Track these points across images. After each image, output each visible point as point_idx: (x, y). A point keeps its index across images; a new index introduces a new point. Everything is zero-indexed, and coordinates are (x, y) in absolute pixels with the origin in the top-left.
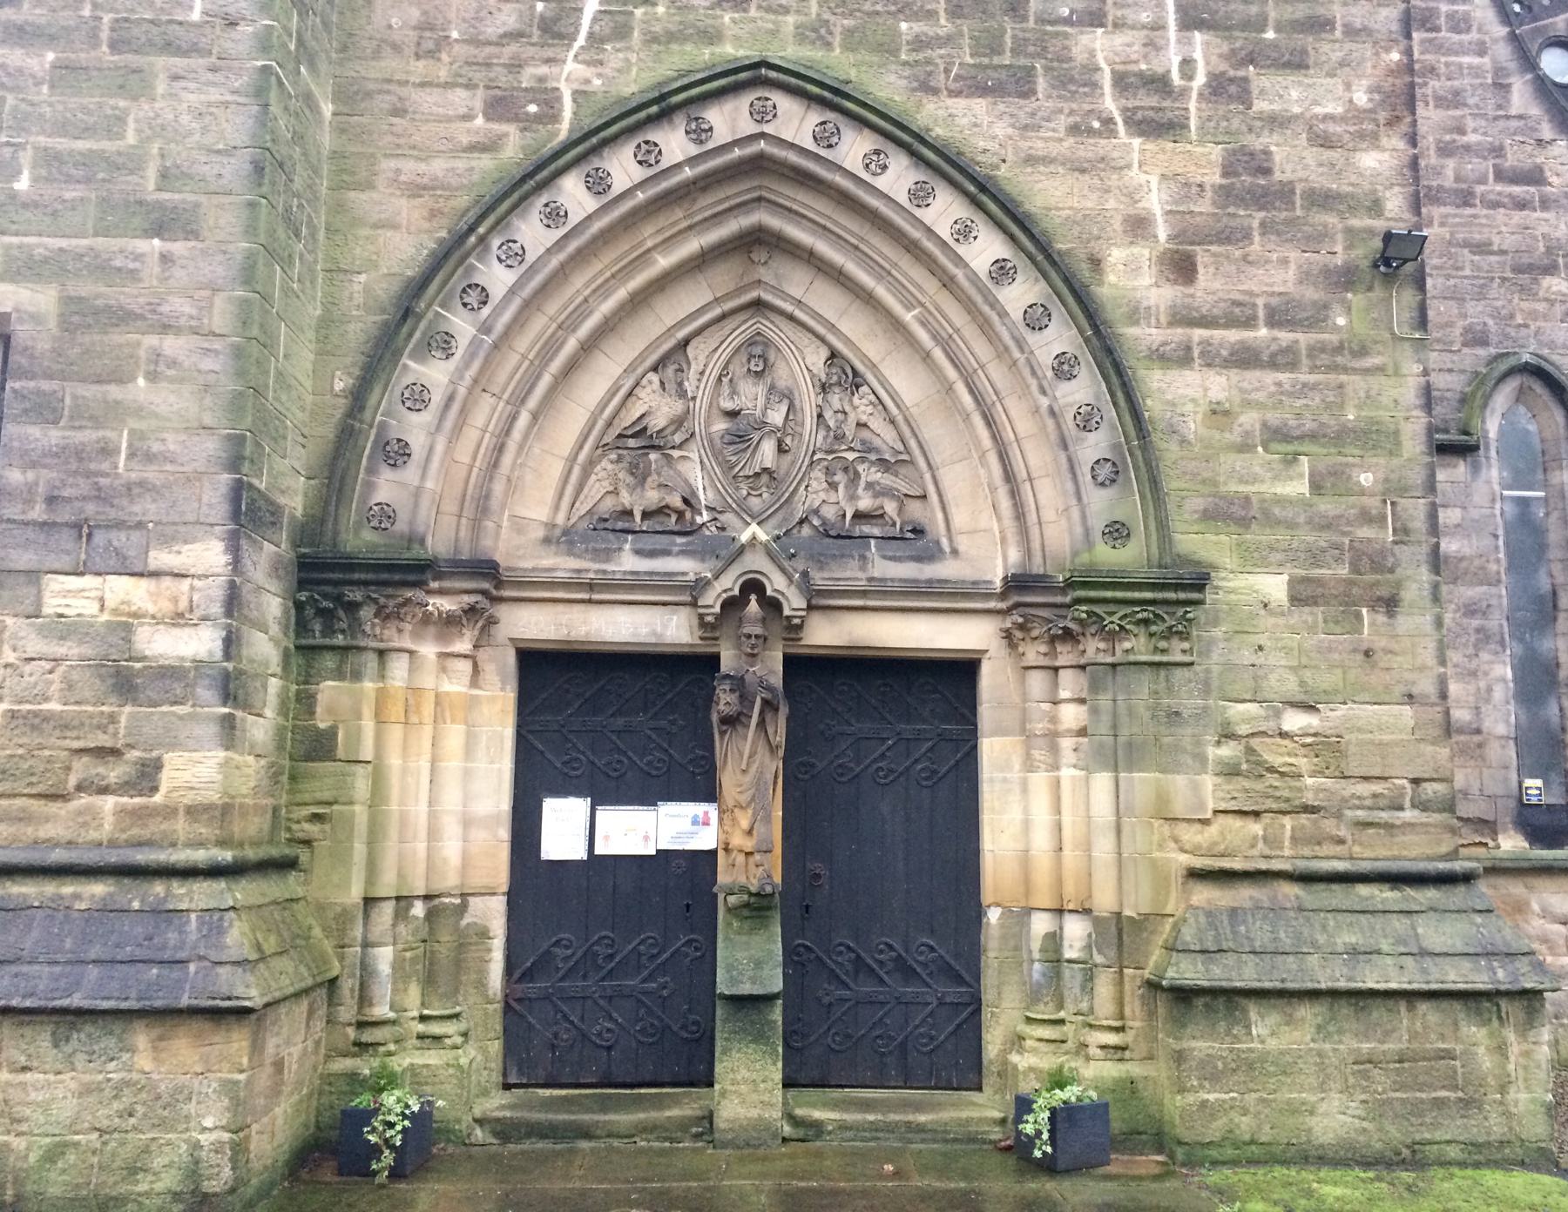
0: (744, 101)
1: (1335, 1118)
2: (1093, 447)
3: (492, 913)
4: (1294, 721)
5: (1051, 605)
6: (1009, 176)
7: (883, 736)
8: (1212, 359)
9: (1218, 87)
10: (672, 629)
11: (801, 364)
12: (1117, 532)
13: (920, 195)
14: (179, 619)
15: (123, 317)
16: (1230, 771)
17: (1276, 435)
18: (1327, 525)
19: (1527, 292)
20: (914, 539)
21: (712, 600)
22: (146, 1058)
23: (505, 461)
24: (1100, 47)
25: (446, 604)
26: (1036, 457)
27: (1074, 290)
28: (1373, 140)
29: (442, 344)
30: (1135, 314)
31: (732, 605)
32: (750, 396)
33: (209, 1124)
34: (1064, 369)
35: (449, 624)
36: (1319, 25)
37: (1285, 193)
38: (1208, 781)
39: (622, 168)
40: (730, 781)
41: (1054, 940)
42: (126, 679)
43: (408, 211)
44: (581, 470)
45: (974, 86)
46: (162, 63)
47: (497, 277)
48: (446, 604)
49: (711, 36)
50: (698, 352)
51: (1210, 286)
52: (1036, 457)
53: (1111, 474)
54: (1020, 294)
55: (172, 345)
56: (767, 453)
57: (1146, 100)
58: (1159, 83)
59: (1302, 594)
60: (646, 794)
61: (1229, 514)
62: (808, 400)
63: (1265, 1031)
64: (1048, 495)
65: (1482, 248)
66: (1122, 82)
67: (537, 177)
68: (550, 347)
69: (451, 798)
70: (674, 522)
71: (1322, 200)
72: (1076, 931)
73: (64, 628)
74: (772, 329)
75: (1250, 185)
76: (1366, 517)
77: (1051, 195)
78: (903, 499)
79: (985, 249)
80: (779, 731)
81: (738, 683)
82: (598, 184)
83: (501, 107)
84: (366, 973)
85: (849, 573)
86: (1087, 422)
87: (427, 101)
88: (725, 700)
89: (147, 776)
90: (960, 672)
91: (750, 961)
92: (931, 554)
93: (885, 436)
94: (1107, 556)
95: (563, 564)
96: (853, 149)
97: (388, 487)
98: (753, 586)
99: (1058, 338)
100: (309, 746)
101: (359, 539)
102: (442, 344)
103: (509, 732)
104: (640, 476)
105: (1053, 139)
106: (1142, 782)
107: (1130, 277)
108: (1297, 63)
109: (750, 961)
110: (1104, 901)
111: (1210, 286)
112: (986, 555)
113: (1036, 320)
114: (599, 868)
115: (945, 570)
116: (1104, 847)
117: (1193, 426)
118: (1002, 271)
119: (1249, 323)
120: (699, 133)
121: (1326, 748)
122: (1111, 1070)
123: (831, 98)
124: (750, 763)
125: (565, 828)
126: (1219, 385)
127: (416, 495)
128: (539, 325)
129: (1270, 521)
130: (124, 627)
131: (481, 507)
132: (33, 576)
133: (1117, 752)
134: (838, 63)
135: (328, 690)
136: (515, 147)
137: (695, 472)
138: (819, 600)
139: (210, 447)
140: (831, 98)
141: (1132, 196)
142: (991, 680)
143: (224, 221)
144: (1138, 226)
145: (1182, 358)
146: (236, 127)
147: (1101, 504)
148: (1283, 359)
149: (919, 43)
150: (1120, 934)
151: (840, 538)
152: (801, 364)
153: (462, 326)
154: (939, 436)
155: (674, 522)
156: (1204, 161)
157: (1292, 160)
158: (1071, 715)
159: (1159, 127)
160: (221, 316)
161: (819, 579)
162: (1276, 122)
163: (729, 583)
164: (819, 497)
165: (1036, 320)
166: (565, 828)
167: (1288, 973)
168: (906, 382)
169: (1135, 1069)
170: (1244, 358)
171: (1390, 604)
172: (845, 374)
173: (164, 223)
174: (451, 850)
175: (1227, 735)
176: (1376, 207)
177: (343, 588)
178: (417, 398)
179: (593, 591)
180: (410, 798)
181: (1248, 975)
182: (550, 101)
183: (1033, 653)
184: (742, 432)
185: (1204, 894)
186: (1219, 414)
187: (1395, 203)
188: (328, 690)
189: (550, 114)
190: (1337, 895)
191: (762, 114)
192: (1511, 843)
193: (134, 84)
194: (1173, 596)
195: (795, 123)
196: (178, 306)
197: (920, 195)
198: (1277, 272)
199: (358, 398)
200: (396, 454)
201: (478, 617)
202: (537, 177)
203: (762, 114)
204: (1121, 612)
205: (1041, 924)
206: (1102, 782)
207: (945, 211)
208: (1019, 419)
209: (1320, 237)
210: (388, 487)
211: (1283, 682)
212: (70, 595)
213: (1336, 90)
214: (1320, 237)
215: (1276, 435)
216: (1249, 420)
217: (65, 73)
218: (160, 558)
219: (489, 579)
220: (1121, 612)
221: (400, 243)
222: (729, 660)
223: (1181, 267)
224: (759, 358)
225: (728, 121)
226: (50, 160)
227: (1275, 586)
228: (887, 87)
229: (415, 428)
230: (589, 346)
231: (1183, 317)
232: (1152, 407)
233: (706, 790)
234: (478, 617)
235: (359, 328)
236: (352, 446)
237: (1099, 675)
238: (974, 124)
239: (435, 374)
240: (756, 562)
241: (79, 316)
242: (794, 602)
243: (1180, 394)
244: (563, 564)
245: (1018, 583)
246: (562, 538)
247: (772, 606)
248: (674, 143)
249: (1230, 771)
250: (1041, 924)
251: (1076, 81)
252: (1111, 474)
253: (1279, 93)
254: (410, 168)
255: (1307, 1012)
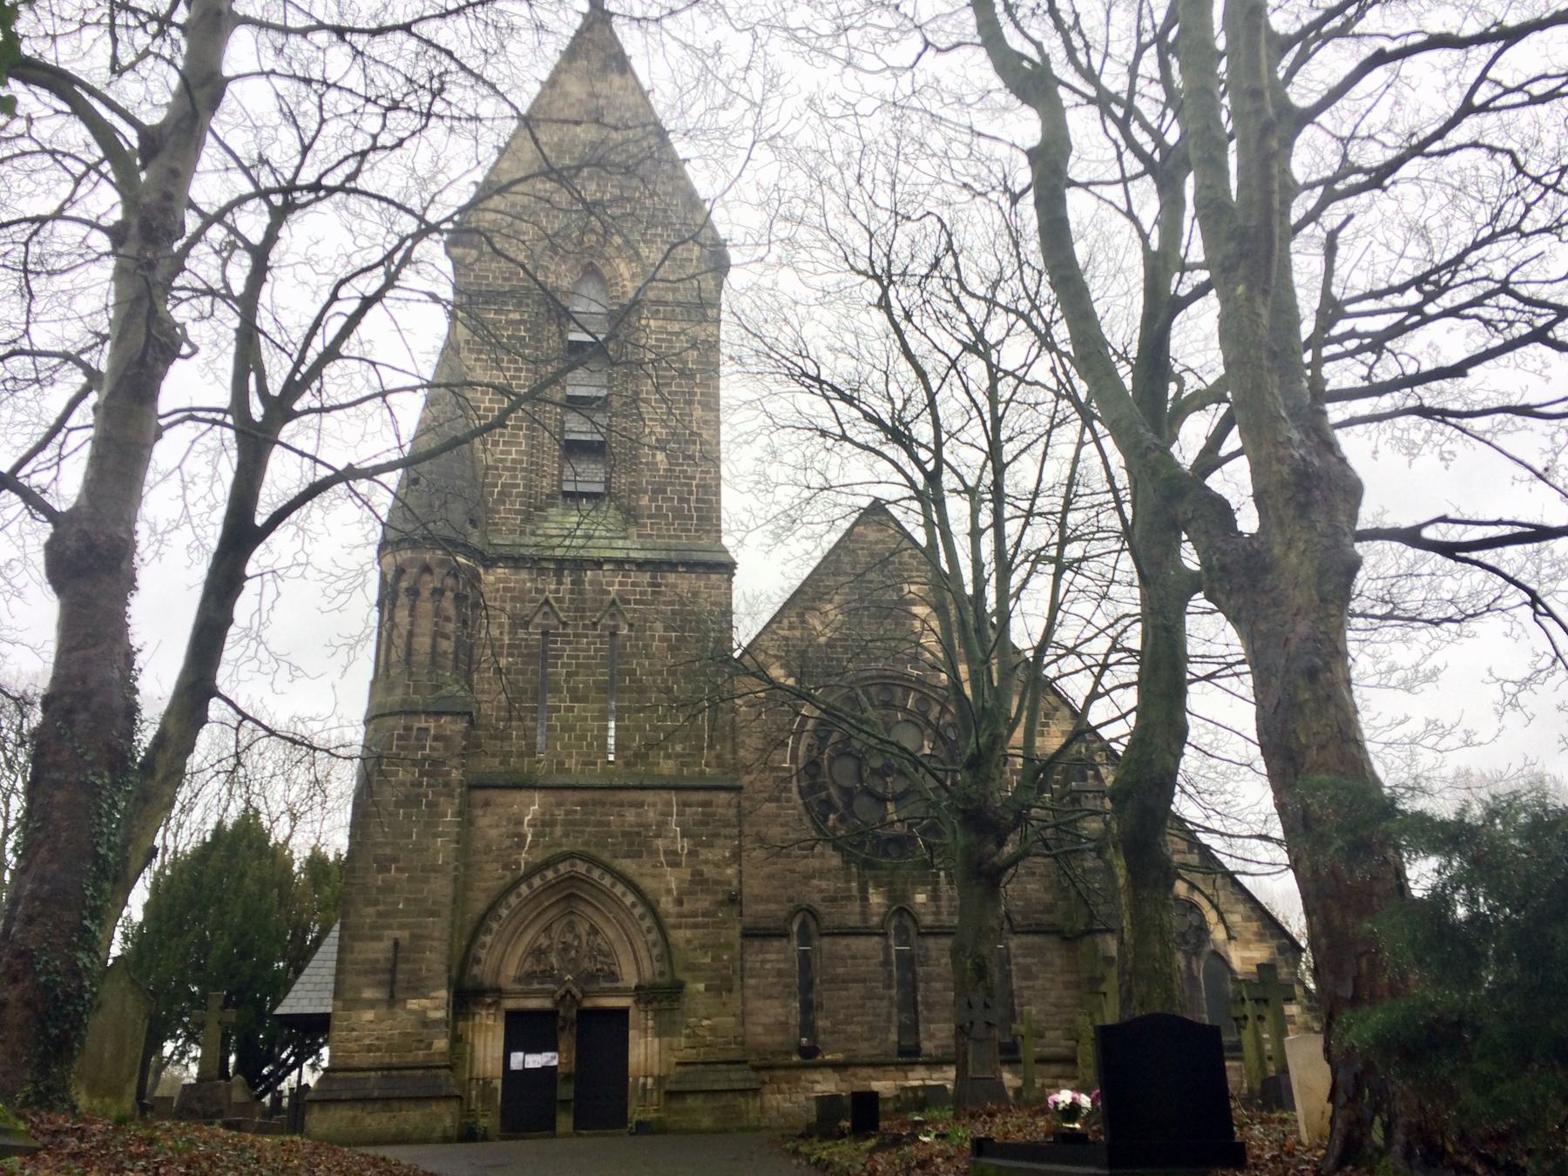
0: (567, 863)
1: (707, 1122)
2: (656, 951)
3: (498, 1083)
4: (705, 1022)
5: (644, 994)
6: (637, 880)
7: (602, 1035)
8: (687, 927)
9: (690, 853)
10: (547, 1004)
11: (583, 928)
12: (662, 974)
13: (613, 885)
14: (436, 1009)
15: (421, 937)
16: (688, 1036)
17: (702, 946)
18: (714, 970)
19: (807, 885)
20: (613, 976)
21: (558, 996)
22: (435, 1108)
23: (505, 961)
24: (660, 843)
25: (489, 1000)
26: (643, 954)
27: (652, 908)
28: (729, 865)
29: (489, 931)
30: (668, 915)
31: (563, 997)
32: (569, 937)
33: (448, 1122)
34: (649, 931)
35: (489, 1006)
36: (717, 835)
37: (707, 881)
38: (683, 1039)
39: (537, 882)
40: (562, 1046)
41: (645, 1084)
42: (426, 1023)
43: (482, 896)
44: (523, 960)
45: (627, 856)
46: (433, 875)
47: (504, 912)
48: (489, 1000)
49: (561, 845)
50: (555, 926)
51: (687, 907)
52: (643, 954)
53: (660, 958)
54: (638, 911)
55: (435, 944)
56: (573, 953)
57: (671, 858)
58: (675, 853)
59: (707, 989)
60: (539, 1051)
61: (691, 968)
62: (584, 939)
63: (690, 1102)
64: (646, 963)
65: (793, 871)
66: (665, 853)
67: (515, 884)
68: (516, 929)
69: (489, 1050)
70: (547, 975)
71: (717, 882)
72: (650, 1081)
73: (412, 1012)
74: (573, 918)
75: (698, 879)
76: (727, 968)
77: (647, 884)
78: (609, 965)
79: (630, 899)
80: (574, 1030)
81: (564, 1019)
82: (530, 886)
83: (506, 867)
84: (470, 1098)
85: (595, 987)
86: (654, 945)
87: (488, 867)
88: (561, 1023)
89: (430, 1046)
90: (624, 1012)
91: (565, 1092)
92: (617, 980)
93: (605, 947)
94: (658, 980)
95: (518, 987)
96: (596, 874)
97: (476, 970)
98: (568, 992)
99: (648, 922)
100: (457, 1040)
101: (469, 984)
102: (489, 931)
103: (502, 1034)
104: (539, 961)
105: (647, 869)
106: (666, 1040)
107: (666, 904)
108: (710, 845)
109: (565, 1092)
110: (656, 1072)
111: (687, 907)
112: (631, 980)
113: (642, 917)
114: (527, 1072)
115: (619, 984)
116: (656, 1058)
117: (682, 945)
118: (634, 905)
119: (696, 916)
120: (556, 871)
121: (712, 1029)
122: (654, 1115)
123: (592, 861)
124: (567, 1040)
125: (517, 1060)
126: (688, 933)
127: (482, 971)
128: (514, 923)
129: (700, 970)
130: (425, 1010)
131: (498, 973)
132: (405, 1001)
133: (659, 1033)
134: (593, 851)
135: (461, 1024)
136: (509, 876)
137: (554, 960)
138: (585, 995)
139: (443, 967)
140: (592, 861)
141: (668, 883)
142: (631, 1013)
143: (447, 912)
144: (669, 891)
145: (679, 926)
146: (449, 891)
147: (657, 965)
148: (705, 926)
149: (613, 844)
150: (659, 1080)
151: (592, 977)
152: (583, 928)
153: (495, 926)
154: (619, 948)
155: (547, 975)
156: (686, 874)
157: (709, 872)
158: (651, 1023)
159: (675, 864)
160: (446, 936)
161: (586, 988)
162: (706, 862)
163: (562, 991)
164: (587, 965)
165: (642, 917)
166: (517, 1060)
167: (698, 1086)
168: (610, 933)
169: (661, 1115)
170: (696, 926)
171: (730, 991)
172: (594, 931)
173: (433, 914)
174: (489, 1066)
175: (688, 1027)
176: (730, 884)
177: (467, 997)
178: (483, 946)
179: (526, 994)
180: (480, 1052)
181: (688, 1087)
182: (518, 864)
183: (641, 1006)
184: (566, 948)
185: (679, 1069)
186: (689, 941)
187: (735, 882)
188: (461, 1024)
189: (519, 868)
190: (713, 1067)
191: (573, 865)
192: (796, 1058)
193: (426, 880)
194: (675, 990)
195: (581, 868)
196: (436, 934)
197: (613, 885)
198: (704, 902)
199: (469, 947)
200: (478, 961)
201: (496, 1003)
202: (515, 884)
203: (573, 865)
204: (663, 996)
205: (641, 1080)
206: (656, 1040)
207: (619, 889)
208: (639, 944)
209: (716, 892)
210: (476, 970)
211: (702, 1012)
212: (413, 1004)
213: (721, 852)
214: (716, 892)
215: (702, 946)
216: (696, 942)
217: (410, 879)
218: (433, 994)
219: (499, 992)
220: (663, 996)
221: (480, 906)
222: (561, 1013)
223: (679, 902)
224: (571, 926)
225: (563, 868)
226: (407, 901)
227: (701, 987)
228: (605, 857)
229: (483, 954)
230: (526, 928)
231: (680, 916)
232: (671, 940)
233: (552, 1047)
234: (496, 1003)
235: (469, 928)
236: (466, 959)
237: (657, 1012)
238: (628, 866)
239: (488, 939)
240: (570, 985)
241: (414, 937)
242: (579, 996)
243: (679, 936)
244: (518, 987)
245: (638, 988)
246: (518, 980)
247: (573, 997)
248: (550, 874)
249: (688, 1036)
250: (641, 1080)
251: (654, 853)
252: (660, 958)
253: (705, 854)
254: (483, 885)
255: (701, 1097)
